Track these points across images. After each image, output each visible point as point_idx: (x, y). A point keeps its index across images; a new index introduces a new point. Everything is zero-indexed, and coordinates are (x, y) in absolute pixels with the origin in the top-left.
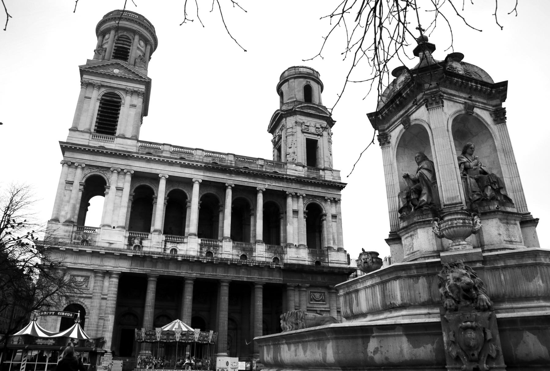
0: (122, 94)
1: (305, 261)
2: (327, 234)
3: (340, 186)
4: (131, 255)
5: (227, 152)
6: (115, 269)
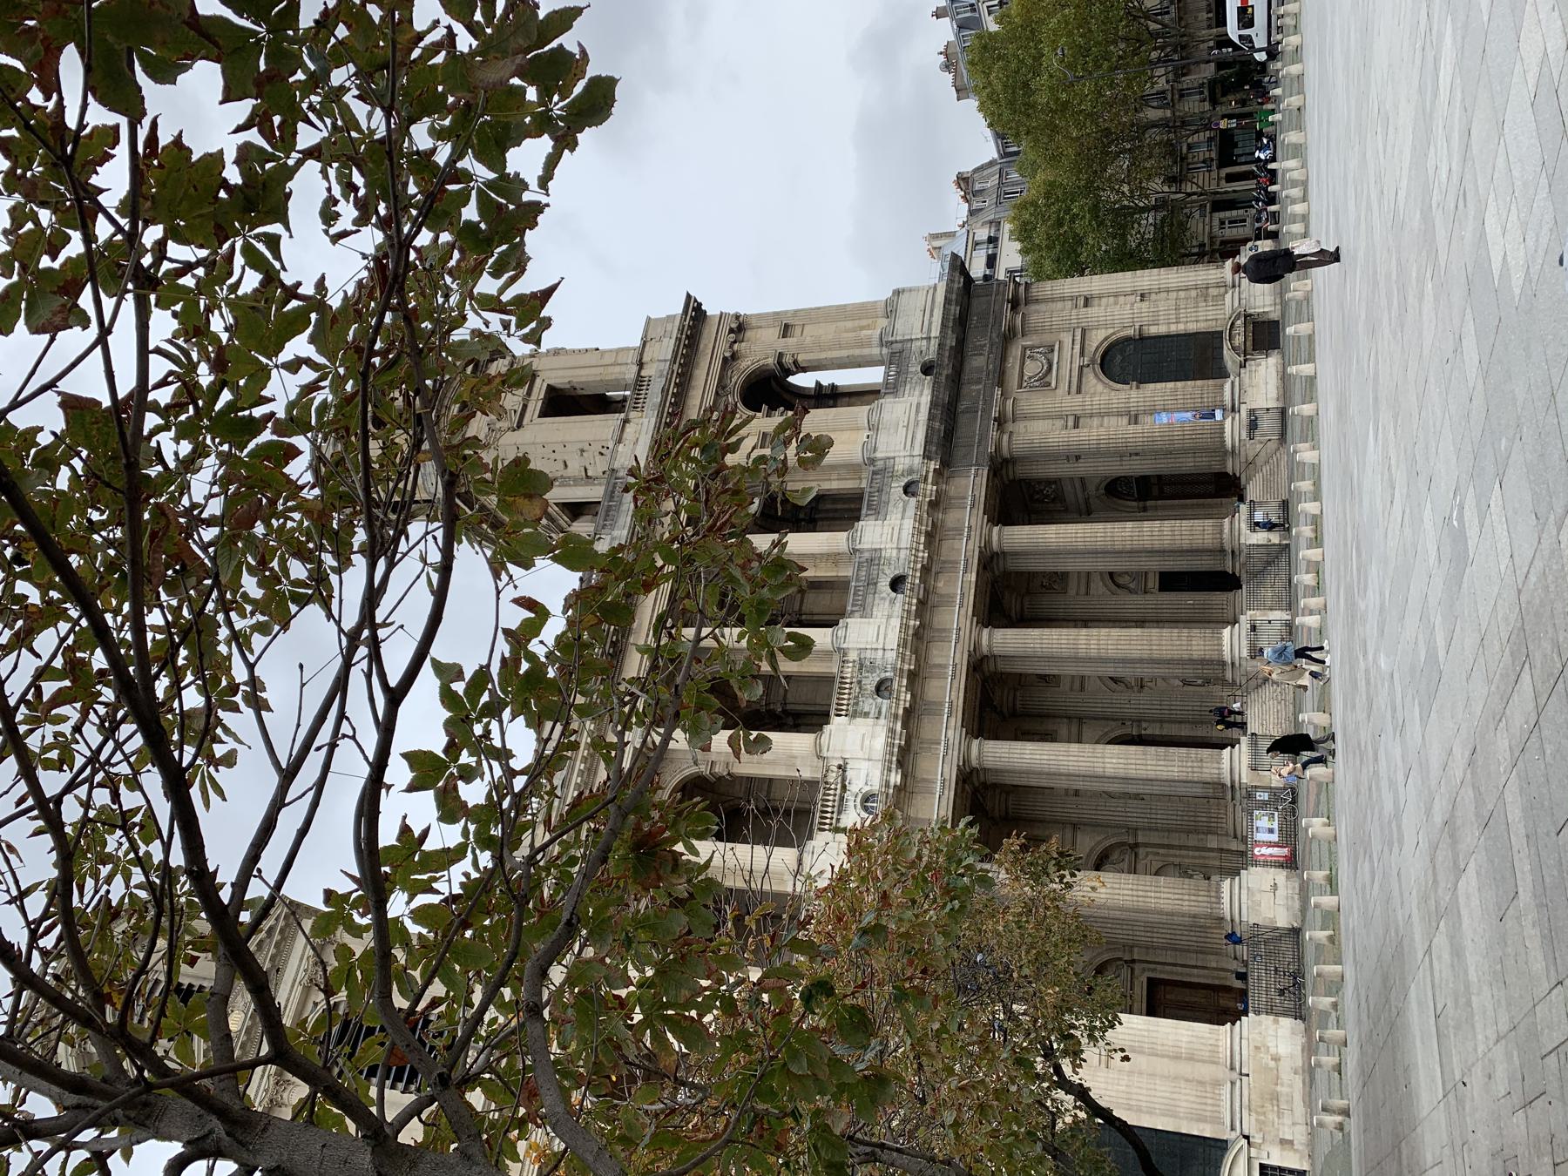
1: (918, 405)
2: (841, 348)
3: (695, 313)
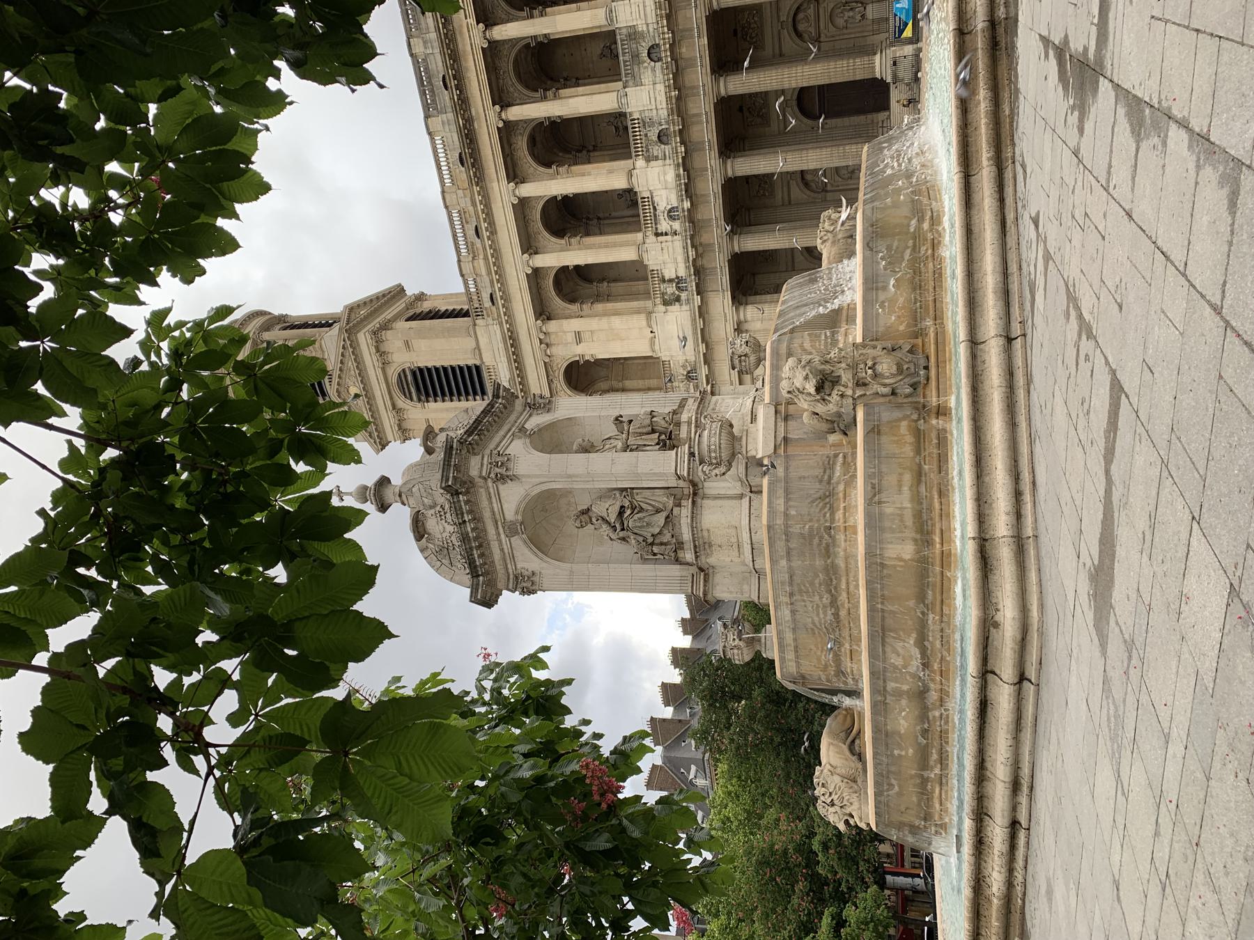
0: (393, 372)
4: (697, 299)
5: (427, 137)
6: (729, 317)
